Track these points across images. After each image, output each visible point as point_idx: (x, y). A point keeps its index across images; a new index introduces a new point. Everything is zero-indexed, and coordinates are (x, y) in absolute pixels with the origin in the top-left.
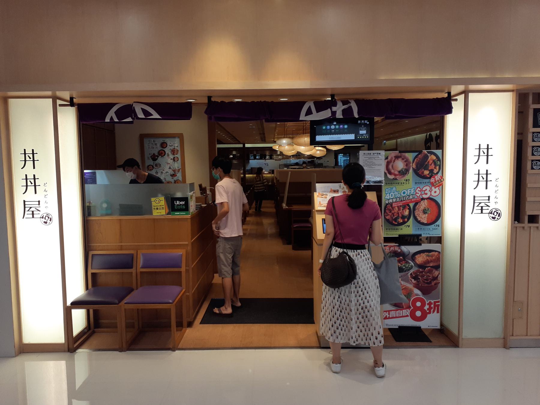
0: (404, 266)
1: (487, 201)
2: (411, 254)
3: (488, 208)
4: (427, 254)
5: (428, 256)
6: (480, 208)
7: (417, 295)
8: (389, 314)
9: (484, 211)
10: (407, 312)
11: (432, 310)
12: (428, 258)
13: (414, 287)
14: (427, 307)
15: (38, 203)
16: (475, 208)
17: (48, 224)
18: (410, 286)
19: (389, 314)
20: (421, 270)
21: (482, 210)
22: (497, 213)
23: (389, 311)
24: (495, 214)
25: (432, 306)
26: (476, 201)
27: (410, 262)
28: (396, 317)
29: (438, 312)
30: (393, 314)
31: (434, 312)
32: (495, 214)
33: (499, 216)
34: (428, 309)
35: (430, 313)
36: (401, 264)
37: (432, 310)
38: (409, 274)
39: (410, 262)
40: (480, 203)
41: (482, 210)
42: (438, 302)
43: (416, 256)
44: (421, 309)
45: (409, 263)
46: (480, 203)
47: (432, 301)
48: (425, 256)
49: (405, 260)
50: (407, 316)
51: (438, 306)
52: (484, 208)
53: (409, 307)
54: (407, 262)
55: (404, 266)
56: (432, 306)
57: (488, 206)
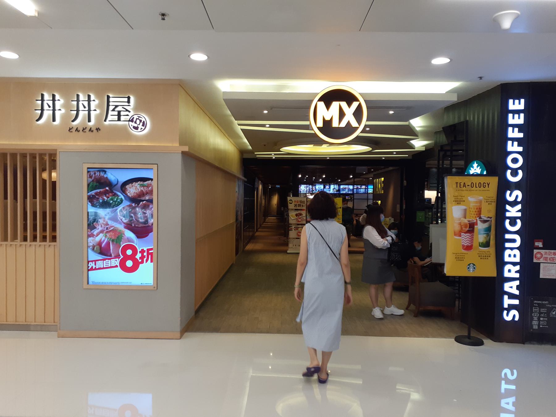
0: (112, 199)
1: (127, 104)
2: (120, 184)
3: (127, 113)
4: (142, 183)
5: (142, 186)
6: (116, 113)
7: (129, 240)
8: (95, 264)
9: (122, 118)
10: (116, 262)
11: (145, 259)
12: (142, 188)
13: (125, 227)
14: (138, 256)
15: (126, 100)
16: (110, 113)
17: (139, 130)
18: (121, 227)
19: (95, 264)
20: (133, 205)
21: (119, 115)
22: (141, 121)
23: (95, 261)
24: (138, 122)
25: (145, 254)
26: (111, 104)
27: (119, 194)
28: (104, 268)
29: (151, 262)
30: (100, 264)
31: (147, 261)
32: (138, 122)
33: (143, 125)
34: (140, 258)
35: (142, 262)
36: (108, 197)
37: (145, 259)
38: (118, 210)
39: (119, 194)
40: (116, 106)
41: (119, 115)
42: (151, 249)
43: (127, 187)
44: (132, 257)
45: (118, 196)
46: (116, 106)
47: (145, 249)
48: (138, 187)
49: (112, 192)
50: (116, 266)
51: (152, 254)
52: (122, 113)
53: (117, 256)
54: (115, 195)
55: (112, 199)
56: (145, 254)
57: (127, 110)
